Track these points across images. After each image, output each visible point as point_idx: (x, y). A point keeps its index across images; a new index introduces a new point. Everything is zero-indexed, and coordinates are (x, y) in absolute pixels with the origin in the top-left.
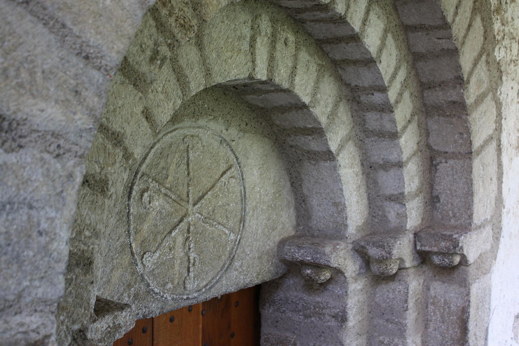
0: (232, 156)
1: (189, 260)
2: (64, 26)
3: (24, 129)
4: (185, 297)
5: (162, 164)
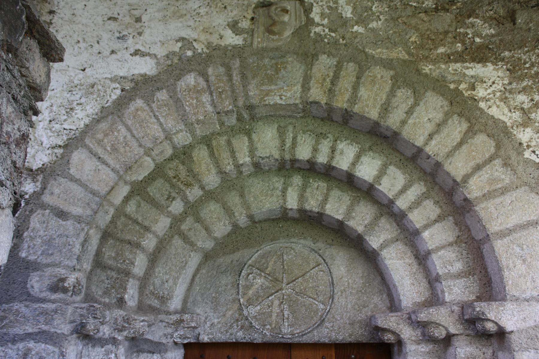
0: (320, 259)
1: (283, 315)
2: (87, 186)
3: (69, 215)
4: (280, 336)
5: (264, 261)
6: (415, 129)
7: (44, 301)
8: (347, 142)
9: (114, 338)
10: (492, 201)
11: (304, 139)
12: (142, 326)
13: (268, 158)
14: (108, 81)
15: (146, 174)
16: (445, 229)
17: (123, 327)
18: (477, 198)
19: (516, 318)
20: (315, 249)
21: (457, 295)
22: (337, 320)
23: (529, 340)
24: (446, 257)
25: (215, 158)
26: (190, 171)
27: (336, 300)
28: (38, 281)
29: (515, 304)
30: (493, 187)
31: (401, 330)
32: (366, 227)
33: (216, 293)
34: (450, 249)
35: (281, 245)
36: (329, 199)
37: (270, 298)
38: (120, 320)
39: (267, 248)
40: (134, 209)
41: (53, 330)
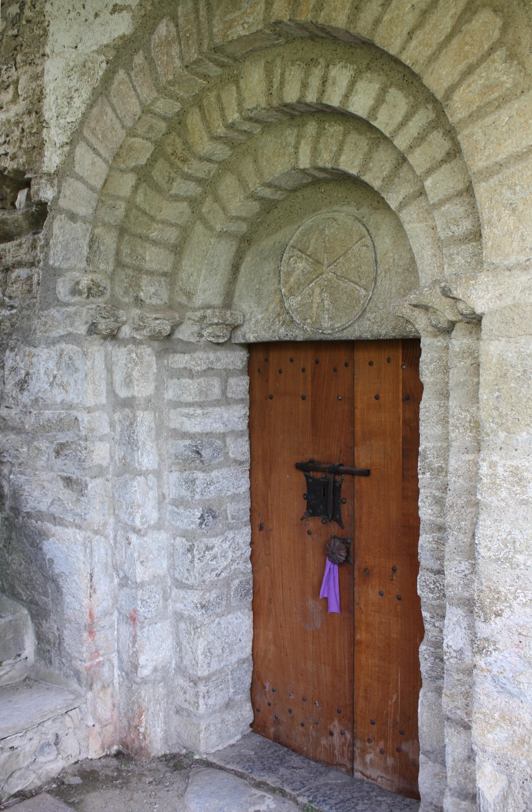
0: (364, 229)
6: (391, 29)
7: (67, 305)
8: (342, 64)
9: (134, 338)
10: (480, 123)
11: (292, 73)
12: (159, 324)
13: (255, 108)
14: (95, 55)
15: (148, 156)
16: (454, 172)
17: (139, 325)
18: (460, 120)
19: (490, 294)
20: (359, 217)
21: (460, 267)
22: (379, 309)
23: (503, 325)
24: (451, 213)
25: (207, 121)
26: (185, 143)
27: (378, 284)
28: (62, 287)
29: (490, 274)
30: (486, 100)
31: (416, 318)
32: (383, 180)
33: (260, 284)
34: (457, 200)
35: (323, 216)
36: (345, 148)
37: (310, 286)
38: (137, 318)
39: (308, 222)
40: (142, 199)
41: (75, 332)
